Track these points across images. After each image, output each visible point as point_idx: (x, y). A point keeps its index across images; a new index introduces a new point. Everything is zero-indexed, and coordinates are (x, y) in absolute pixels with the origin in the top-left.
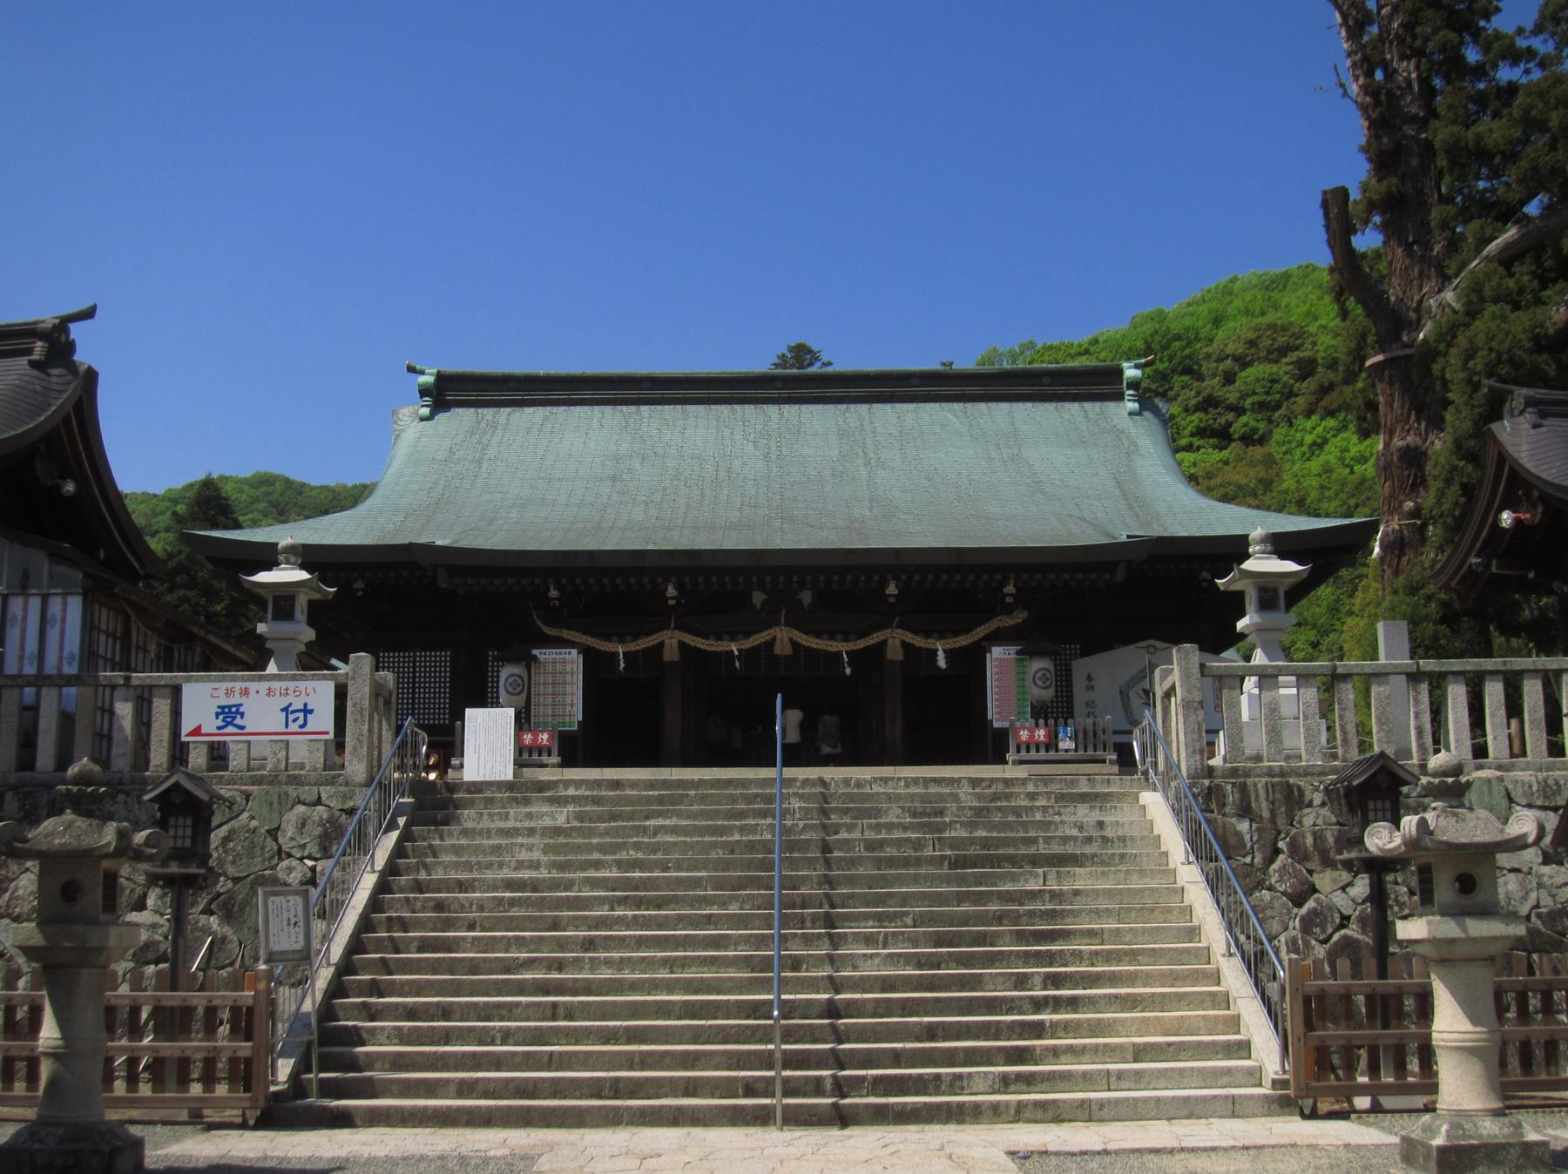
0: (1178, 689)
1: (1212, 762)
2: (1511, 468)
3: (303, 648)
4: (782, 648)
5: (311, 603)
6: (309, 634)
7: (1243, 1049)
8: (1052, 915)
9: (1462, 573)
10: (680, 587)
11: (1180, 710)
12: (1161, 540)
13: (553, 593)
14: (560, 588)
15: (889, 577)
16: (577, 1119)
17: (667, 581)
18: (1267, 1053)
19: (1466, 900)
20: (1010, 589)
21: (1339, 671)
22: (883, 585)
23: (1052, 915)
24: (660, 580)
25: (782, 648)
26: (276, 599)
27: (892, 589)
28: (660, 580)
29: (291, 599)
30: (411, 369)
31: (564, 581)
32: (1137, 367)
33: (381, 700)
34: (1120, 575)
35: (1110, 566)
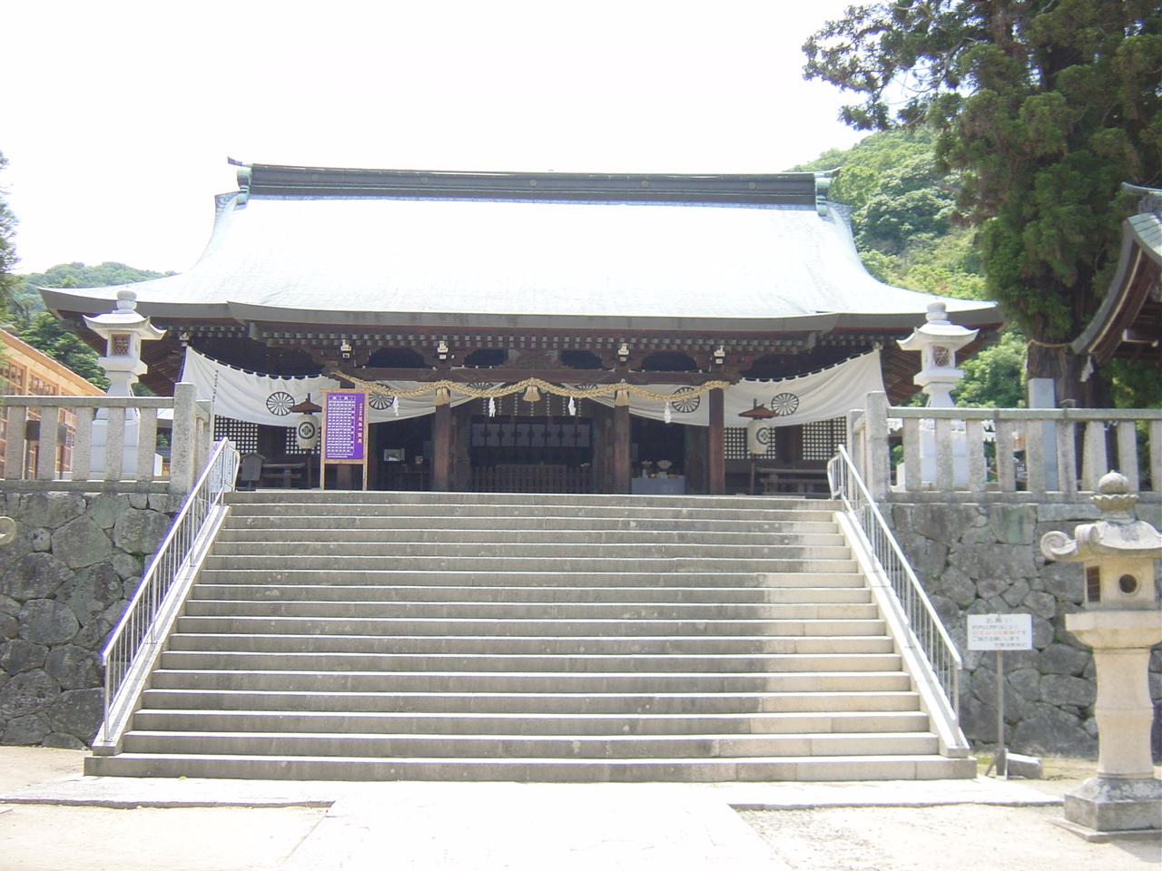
0: (867, 428)
1: (893, 489)
2: (1144, 254)
3: (136, 380)
4: (532, 395)
5: (144, 343)
6: (143, 368)
7: (925, 725)
8: (751, 666)
9: (1098, 341)
10: (450, 345)
11: (869, 446)
12: (842, 316)
13: (345, 347)
14: (352, 344)
15: (622, 340)
16: (366, 774)
17: (439, 339)
18: (948, 732)
19: (1126, 597)
20: (720, 353)
21: (1002, 416)
22: (616, 347)
23: (751, 666)
24: (433, 337)
25: (532, 395)
26: (115, 338)
27: (624, 350)
28: (433, 337)
29: (126, 338)
30: (231, 162)
31: (355, 337)
32: (826, 176)
33: (201, 423)
34: (811, 343)
35: (804, 336)
